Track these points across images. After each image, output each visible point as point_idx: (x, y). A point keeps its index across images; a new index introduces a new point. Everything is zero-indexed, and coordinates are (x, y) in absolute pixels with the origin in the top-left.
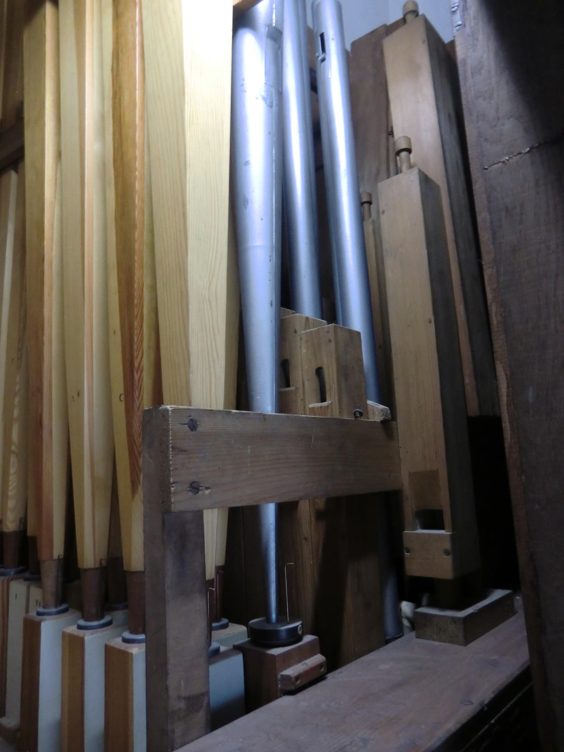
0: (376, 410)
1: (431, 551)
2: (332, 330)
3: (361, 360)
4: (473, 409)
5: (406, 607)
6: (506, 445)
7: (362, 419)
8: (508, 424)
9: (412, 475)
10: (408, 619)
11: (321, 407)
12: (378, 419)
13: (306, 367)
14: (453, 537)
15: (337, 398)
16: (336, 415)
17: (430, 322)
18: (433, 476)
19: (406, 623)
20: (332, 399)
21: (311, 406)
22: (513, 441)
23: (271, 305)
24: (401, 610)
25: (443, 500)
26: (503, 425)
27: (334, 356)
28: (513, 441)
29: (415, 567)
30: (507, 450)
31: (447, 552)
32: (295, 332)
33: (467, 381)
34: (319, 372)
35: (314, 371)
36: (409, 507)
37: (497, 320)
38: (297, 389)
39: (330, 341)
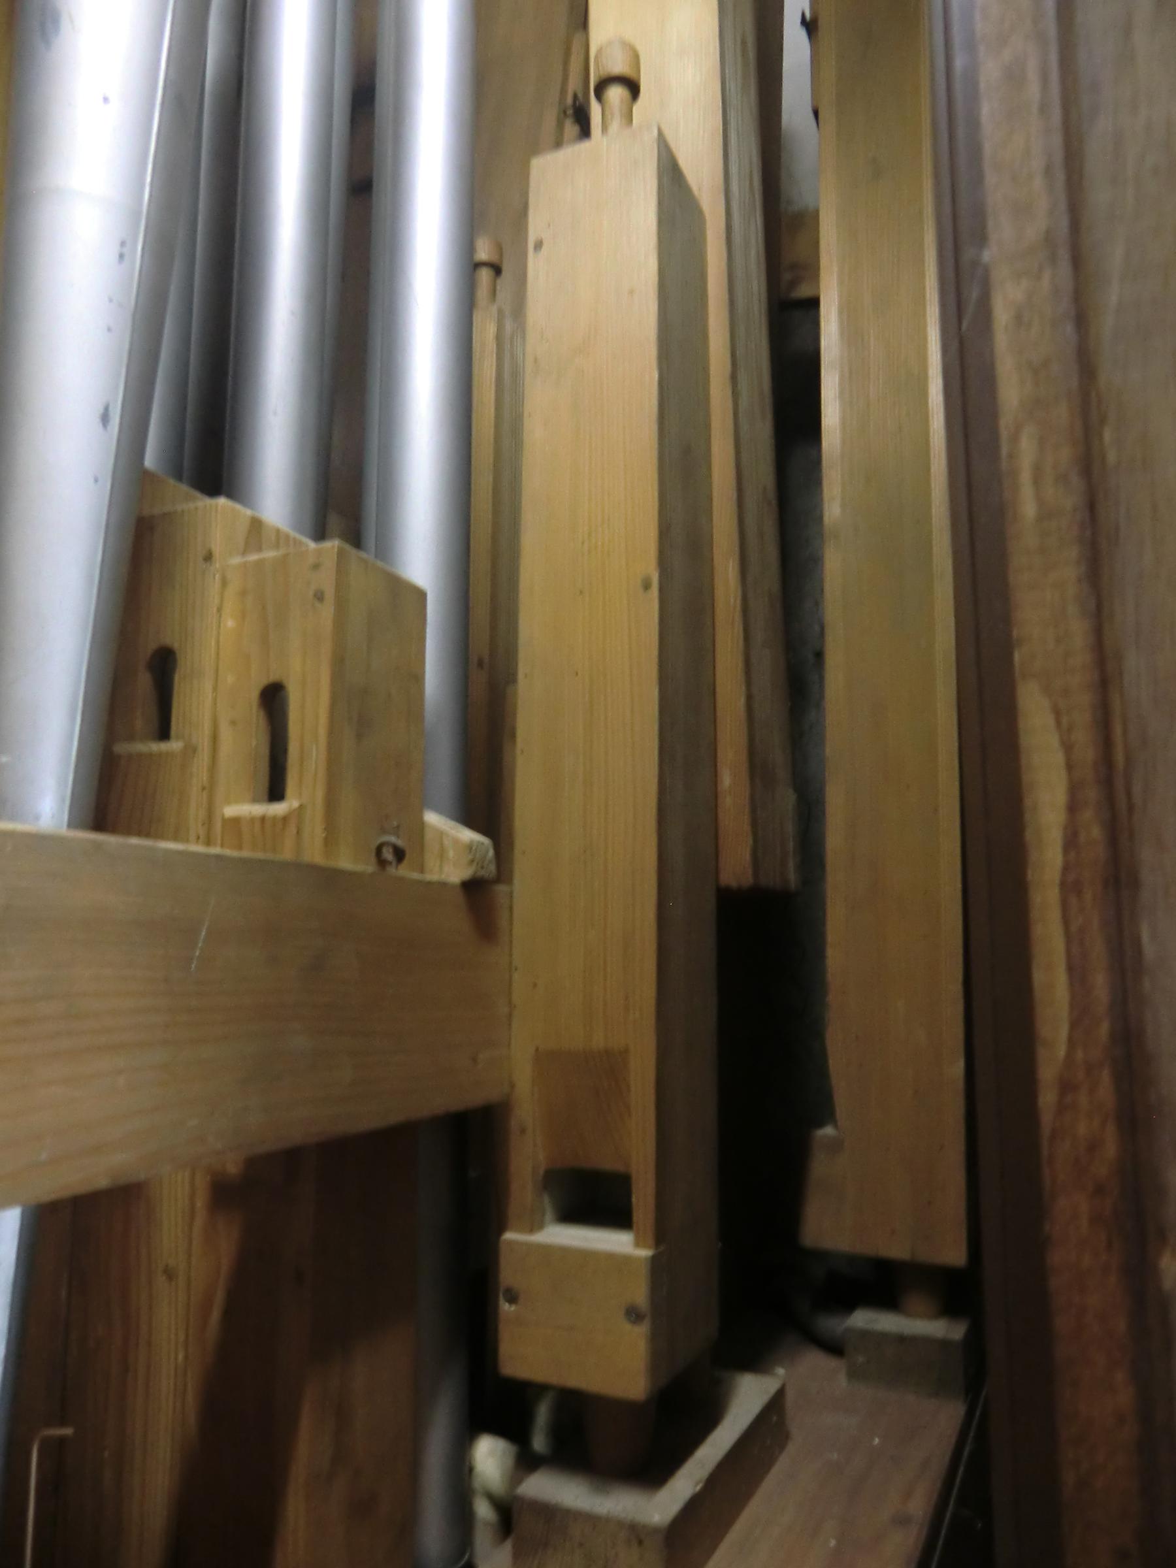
0: (450, 844)
1: (584, 1290)
2: (330, 563)
3: (418, 678)
4: (736, 866)
5: (489, 1456)
6: (1048, 1070)
7: (404, 871)
8: (1061, 978)
9: (546, 1060)
10: (492, 1498)
11: (263, 819)
12: (455, 873)
13: (230, 679)
14: (656, 1266)
15: (320, 794)
16: (314, 854)
17: (647, 586)
18: (607, 1067)
19: (483, 1510)
20: (304, 791)
21: (230, 811)
22: (1079, 1055)
23: (105, 418)
24: (471, 1470)
25: (635, 1147)
26: (1039, 977)
27: (326, 649)
28: (1079, 1055)
29: (528, 1349)
30: (1047, 1098)
31: (634, 1315)
32: (209, 557)
33: (726, 780)
34: (273, 698)
35: (255, 695)
36: (528, 1156)
37: (1040, 500)
38: (191, 750)
39: (319, 596)
